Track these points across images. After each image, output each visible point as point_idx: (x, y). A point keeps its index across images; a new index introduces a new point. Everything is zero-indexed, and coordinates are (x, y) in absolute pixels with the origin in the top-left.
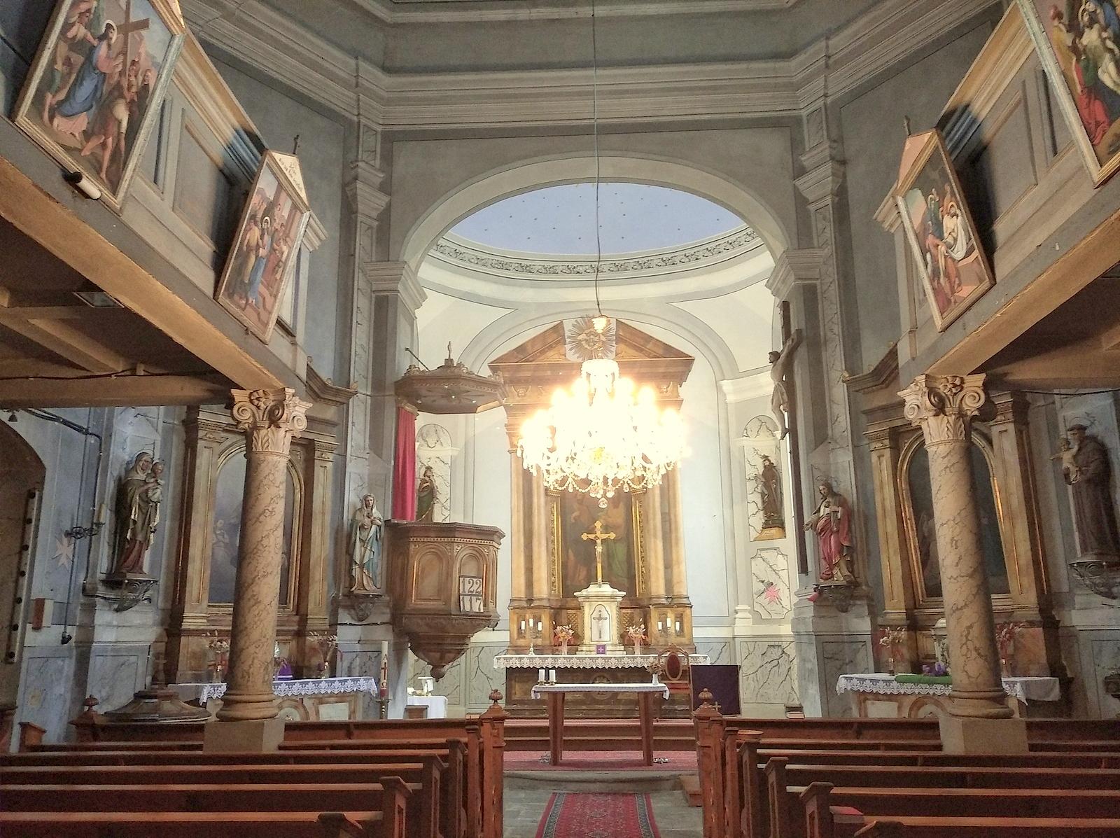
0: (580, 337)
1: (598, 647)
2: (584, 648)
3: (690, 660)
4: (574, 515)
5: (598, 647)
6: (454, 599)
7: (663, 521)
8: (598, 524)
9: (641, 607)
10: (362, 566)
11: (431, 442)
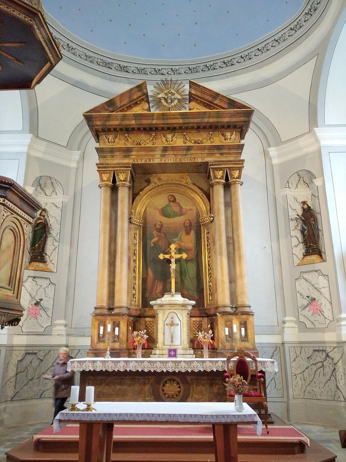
1: (170, 351)
2: (157, 352)
3: (259, 364)
4: (153, 240)
5: (170, 351)
7: (228, 244)
8: (173, 247)
9: (208, 316)
11: (48, 191)
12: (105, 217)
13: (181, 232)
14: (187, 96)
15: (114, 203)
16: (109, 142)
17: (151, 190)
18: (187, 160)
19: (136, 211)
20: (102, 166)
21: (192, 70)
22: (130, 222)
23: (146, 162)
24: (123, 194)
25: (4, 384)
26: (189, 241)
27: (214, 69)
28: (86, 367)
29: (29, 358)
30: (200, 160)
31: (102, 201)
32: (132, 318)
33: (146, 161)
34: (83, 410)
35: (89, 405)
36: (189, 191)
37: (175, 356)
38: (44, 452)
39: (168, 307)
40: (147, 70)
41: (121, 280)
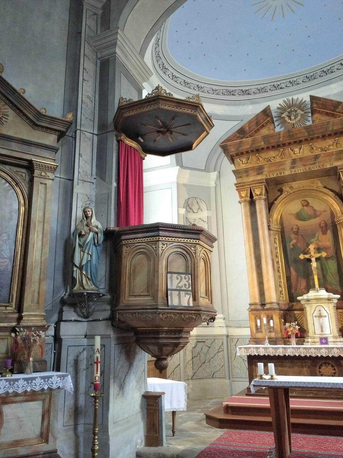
0: (283, 115)
1: (321, 339)
2: (310, 340)
4: (292, 243)
5: (321, 339)
6: (161, 294)
8: (312, 247)
10: (81, 268)
12: (247, 228)
13: (318, 233)
14: (308, 110)
15: (253, 214)
16: (243, 164)
17: (284, 198)
18: (316, 168)
19: (273, 219)
20: (240, 185)
21: (310, 78)
22: (269, 229)
23: (277, 176)
24: (261, 206)
25: (185, 366)
26: (327, 240)
27: (332, 72)
28: (251, 352)
29: (200, 345)
30: (328, 166)
31: (243, 214)
32: (282, 312)
33: (277, 174)
34: (268, 379)
35: (272, 376)
36: (321, 194)
37: (327, 343)
38: (232, 414)
39: (314, 301)
40: (267, 88)
41: (268, 280)
